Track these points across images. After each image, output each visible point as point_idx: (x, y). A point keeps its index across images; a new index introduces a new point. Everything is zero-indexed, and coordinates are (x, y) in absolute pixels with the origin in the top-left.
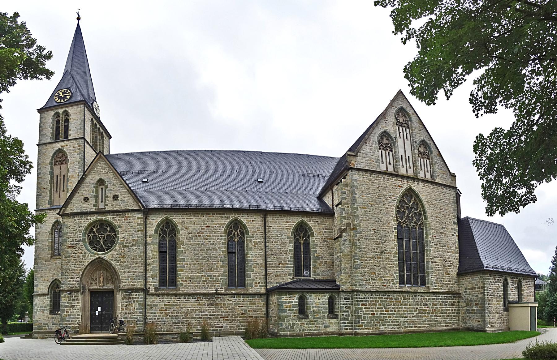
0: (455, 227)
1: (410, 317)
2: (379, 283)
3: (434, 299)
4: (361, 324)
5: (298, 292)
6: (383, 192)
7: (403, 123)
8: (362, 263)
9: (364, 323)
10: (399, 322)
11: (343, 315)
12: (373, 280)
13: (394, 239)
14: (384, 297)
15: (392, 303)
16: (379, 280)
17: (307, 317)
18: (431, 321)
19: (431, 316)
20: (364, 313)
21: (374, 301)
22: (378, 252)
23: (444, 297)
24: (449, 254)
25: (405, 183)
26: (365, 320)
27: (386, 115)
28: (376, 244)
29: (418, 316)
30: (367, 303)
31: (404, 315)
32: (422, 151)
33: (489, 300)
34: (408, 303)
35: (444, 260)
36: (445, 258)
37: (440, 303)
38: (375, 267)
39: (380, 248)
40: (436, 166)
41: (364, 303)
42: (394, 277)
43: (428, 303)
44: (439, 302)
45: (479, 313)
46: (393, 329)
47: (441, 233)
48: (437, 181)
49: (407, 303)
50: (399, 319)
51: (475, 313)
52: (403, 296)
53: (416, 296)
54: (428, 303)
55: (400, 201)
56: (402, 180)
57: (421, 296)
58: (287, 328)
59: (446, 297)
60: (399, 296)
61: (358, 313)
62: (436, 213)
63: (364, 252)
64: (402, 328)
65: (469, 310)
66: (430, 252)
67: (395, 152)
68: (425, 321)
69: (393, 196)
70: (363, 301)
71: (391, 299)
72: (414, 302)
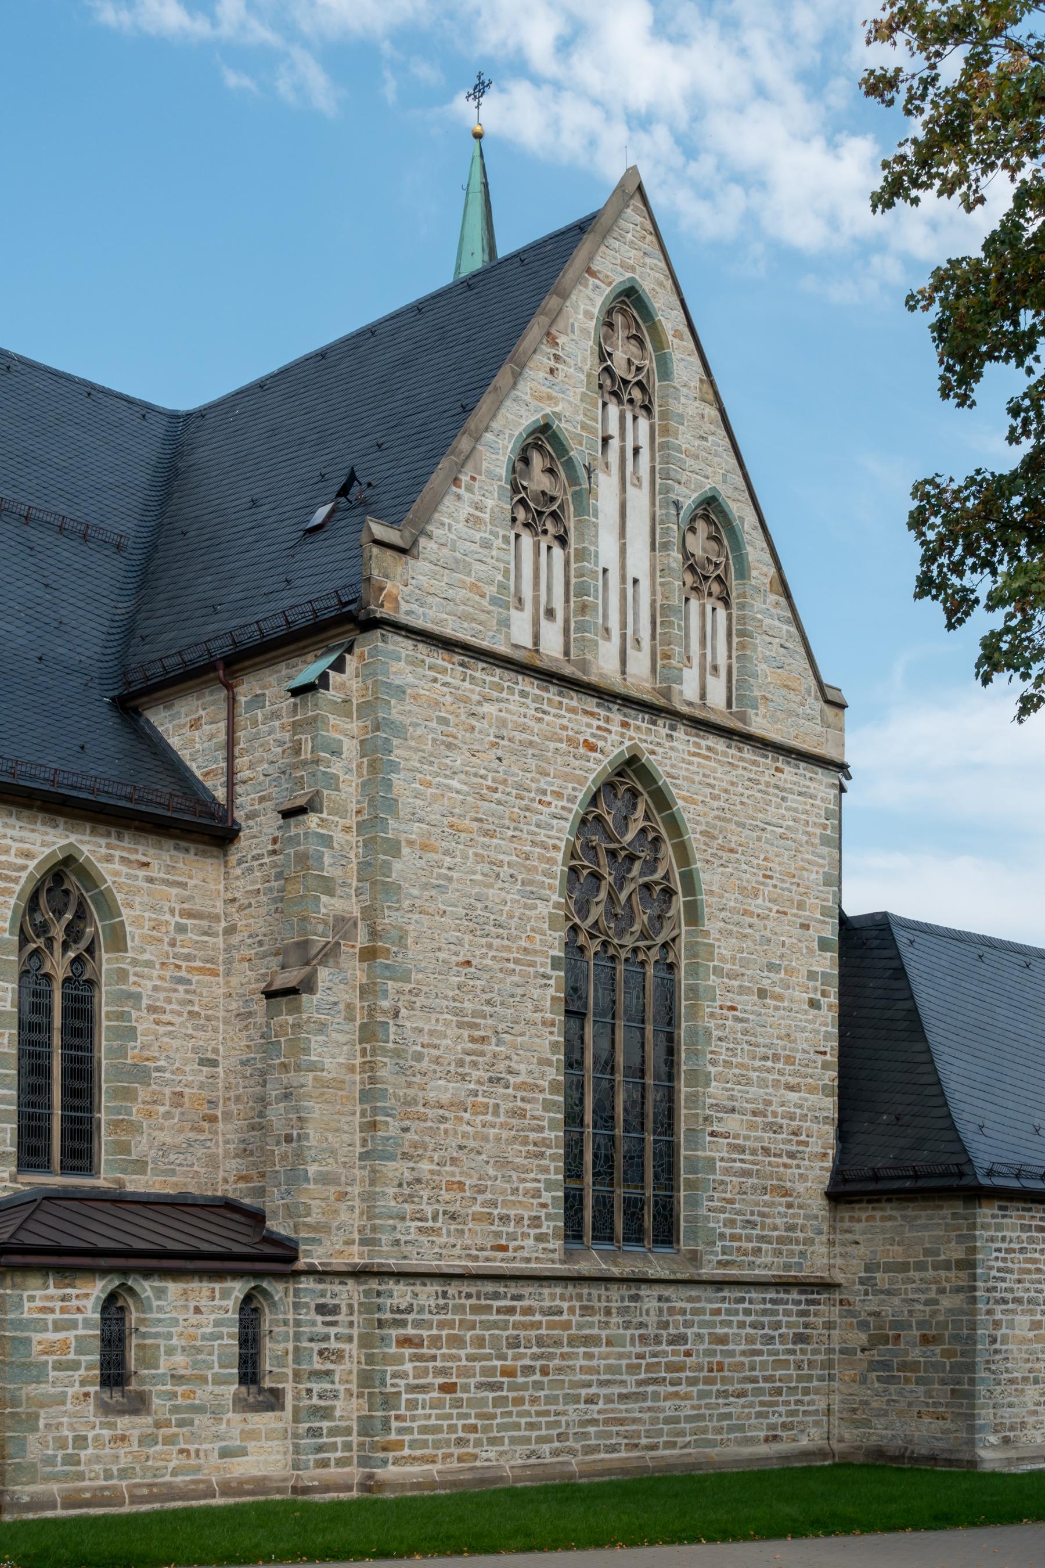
0: (827, 963)
1: (609, 1399)
2: (477, 1235)
3: (717, 1312)
4: (393, 1436)
5: (104, 1272)
6: (515, 769)
7: (626, 382)
8: (406, 1130)
9: (409, 1430)
10: (557, 1424)
11: (309, 1391)
12: (453, 1217)
13: (549, 1016)
14: (496, 1304)
15: (534, 1333)
16: (477, 1218)
17: (139, 1405)
18: (700, 1417)
19: (702, 1395)
20: (412, 1381)
21: (451, 1324)
22: (479, 1082)
23: (764, 1300)
24: (793, 1096)
25: (615, 728)
26: (413, 1418)
27: (560, 324)
28: (473, 1040)
29: (643, 1396)
30: (425, 1333)
31: (584, 1392)
32: (699, 553)
33: (997, 1324)
34: (604, 1334)
35: (777, 1129)
36: (775, 1114)
37: (743, 1332)
38: (462, 1155)
39: (488, 1058)
40: (762, 648)
41: (410, 1331)
42: (544, 1206)
43: (689, 1332)
44: (742, 1325)
45: (943, 1382)
46: (533, 1461)
47: (762, 993)
48: (759, 725)
49: (595, 1331)
50: (560, 1408)
51: (919, 1381)
52: (580, 1297)
53: (635, 1298)
54: (689, 1332)
55: (584, 821)
56: (603, 713)
57: (660, 1299)
58: (50, 1461)
59: (773, 1301)
60: (562, 1298)
61: (383, 1383)
62: (742, 890)
63: (418, 1079)
64: (571, 1451)
65: (885, 1365)
66: (707, 1084)
67: (582, 555)
68: (676, 1420)
69: (558, 795)
70: (403, 1324)
71: (528, 1311)
72: (627, 1325)
